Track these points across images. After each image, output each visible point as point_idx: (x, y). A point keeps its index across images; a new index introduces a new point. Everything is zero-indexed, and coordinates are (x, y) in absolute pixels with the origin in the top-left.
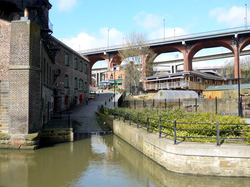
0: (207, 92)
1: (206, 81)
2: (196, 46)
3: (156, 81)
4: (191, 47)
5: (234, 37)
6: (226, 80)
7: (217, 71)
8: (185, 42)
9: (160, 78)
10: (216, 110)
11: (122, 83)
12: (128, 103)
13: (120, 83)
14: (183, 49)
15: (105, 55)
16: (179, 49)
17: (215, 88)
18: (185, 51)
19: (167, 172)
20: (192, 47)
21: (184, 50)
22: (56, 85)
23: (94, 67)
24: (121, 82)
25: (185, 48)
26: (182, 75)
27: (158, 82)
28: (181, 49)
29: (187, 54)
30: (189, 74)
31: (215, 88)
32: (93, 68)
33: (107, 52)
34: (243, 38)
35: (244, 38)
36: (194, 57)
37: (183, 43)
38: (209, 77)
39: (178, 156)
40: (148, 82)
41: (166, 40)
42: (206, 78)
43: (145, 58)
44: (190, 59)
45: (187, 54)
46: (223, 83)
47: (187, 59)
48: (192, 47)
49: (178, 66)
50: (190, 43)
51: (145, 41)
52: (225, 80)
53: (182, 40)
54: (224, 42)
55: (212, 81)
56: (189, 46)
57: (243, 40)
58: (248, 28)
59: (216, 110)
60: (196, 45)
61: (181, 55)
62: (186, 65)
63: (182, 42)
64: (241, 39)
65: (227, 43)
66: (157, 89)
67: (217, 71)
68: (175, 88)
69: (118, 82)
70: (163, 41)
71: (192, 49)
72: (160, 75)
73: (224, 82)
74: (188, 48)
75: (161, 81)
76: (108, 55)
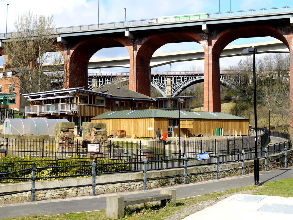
0: (120, 123)
1: (117, 102)
2: (149, 40)
3: (53, 100)
4: (141, 42)
5: (124, 34)
6: (155, 100)
7: (223, 78)
9: (61, 94)
11: (14, 100)
12: (235, 112)
13: (11, 99)
14: (129, 44)
15: (126, 37)
16: (123, 43)
17: (127, 114)
18: (132, 46)
20: (143, 41)
21: (131, 45)
23: (94, 58)
24: (14, 98)
25: (132, 41)
26: (68, 93)
27: (57, 101)
28: (127, 43)
29: (135, 53)
30: (76, 92)
31: (127, 114)
34: (217, 31)
35: (218, 31)
36: (155, 55)
37: (204, 27)
38: (123, 96)
39: (133, 183)
40: (31, 101)
41: (101, 27)
42: (113, 98)
43: (69, 57)
44: (218, 53)
45: (135, 52)
46: (151, 105)
47: (135, 61)
48: (143, 41)
49: (151, 68)
51: (51, 27)
52: (153, 100)
53: (202, 23)
54: (189, 35)
55: (128, 102)
56: (138, 39)
57: (217, 34)
60: (149, 38)
61: (202, 46)
62: (132, 71)
63: (124, 32)
65: (192, 36)
66: (40, 114)
67: (223, 78)
68: (59, 113)
69: (9, 97)
71: (143, 44)
73: (152, 104)
74: (137, 43)
75: (62, 99)
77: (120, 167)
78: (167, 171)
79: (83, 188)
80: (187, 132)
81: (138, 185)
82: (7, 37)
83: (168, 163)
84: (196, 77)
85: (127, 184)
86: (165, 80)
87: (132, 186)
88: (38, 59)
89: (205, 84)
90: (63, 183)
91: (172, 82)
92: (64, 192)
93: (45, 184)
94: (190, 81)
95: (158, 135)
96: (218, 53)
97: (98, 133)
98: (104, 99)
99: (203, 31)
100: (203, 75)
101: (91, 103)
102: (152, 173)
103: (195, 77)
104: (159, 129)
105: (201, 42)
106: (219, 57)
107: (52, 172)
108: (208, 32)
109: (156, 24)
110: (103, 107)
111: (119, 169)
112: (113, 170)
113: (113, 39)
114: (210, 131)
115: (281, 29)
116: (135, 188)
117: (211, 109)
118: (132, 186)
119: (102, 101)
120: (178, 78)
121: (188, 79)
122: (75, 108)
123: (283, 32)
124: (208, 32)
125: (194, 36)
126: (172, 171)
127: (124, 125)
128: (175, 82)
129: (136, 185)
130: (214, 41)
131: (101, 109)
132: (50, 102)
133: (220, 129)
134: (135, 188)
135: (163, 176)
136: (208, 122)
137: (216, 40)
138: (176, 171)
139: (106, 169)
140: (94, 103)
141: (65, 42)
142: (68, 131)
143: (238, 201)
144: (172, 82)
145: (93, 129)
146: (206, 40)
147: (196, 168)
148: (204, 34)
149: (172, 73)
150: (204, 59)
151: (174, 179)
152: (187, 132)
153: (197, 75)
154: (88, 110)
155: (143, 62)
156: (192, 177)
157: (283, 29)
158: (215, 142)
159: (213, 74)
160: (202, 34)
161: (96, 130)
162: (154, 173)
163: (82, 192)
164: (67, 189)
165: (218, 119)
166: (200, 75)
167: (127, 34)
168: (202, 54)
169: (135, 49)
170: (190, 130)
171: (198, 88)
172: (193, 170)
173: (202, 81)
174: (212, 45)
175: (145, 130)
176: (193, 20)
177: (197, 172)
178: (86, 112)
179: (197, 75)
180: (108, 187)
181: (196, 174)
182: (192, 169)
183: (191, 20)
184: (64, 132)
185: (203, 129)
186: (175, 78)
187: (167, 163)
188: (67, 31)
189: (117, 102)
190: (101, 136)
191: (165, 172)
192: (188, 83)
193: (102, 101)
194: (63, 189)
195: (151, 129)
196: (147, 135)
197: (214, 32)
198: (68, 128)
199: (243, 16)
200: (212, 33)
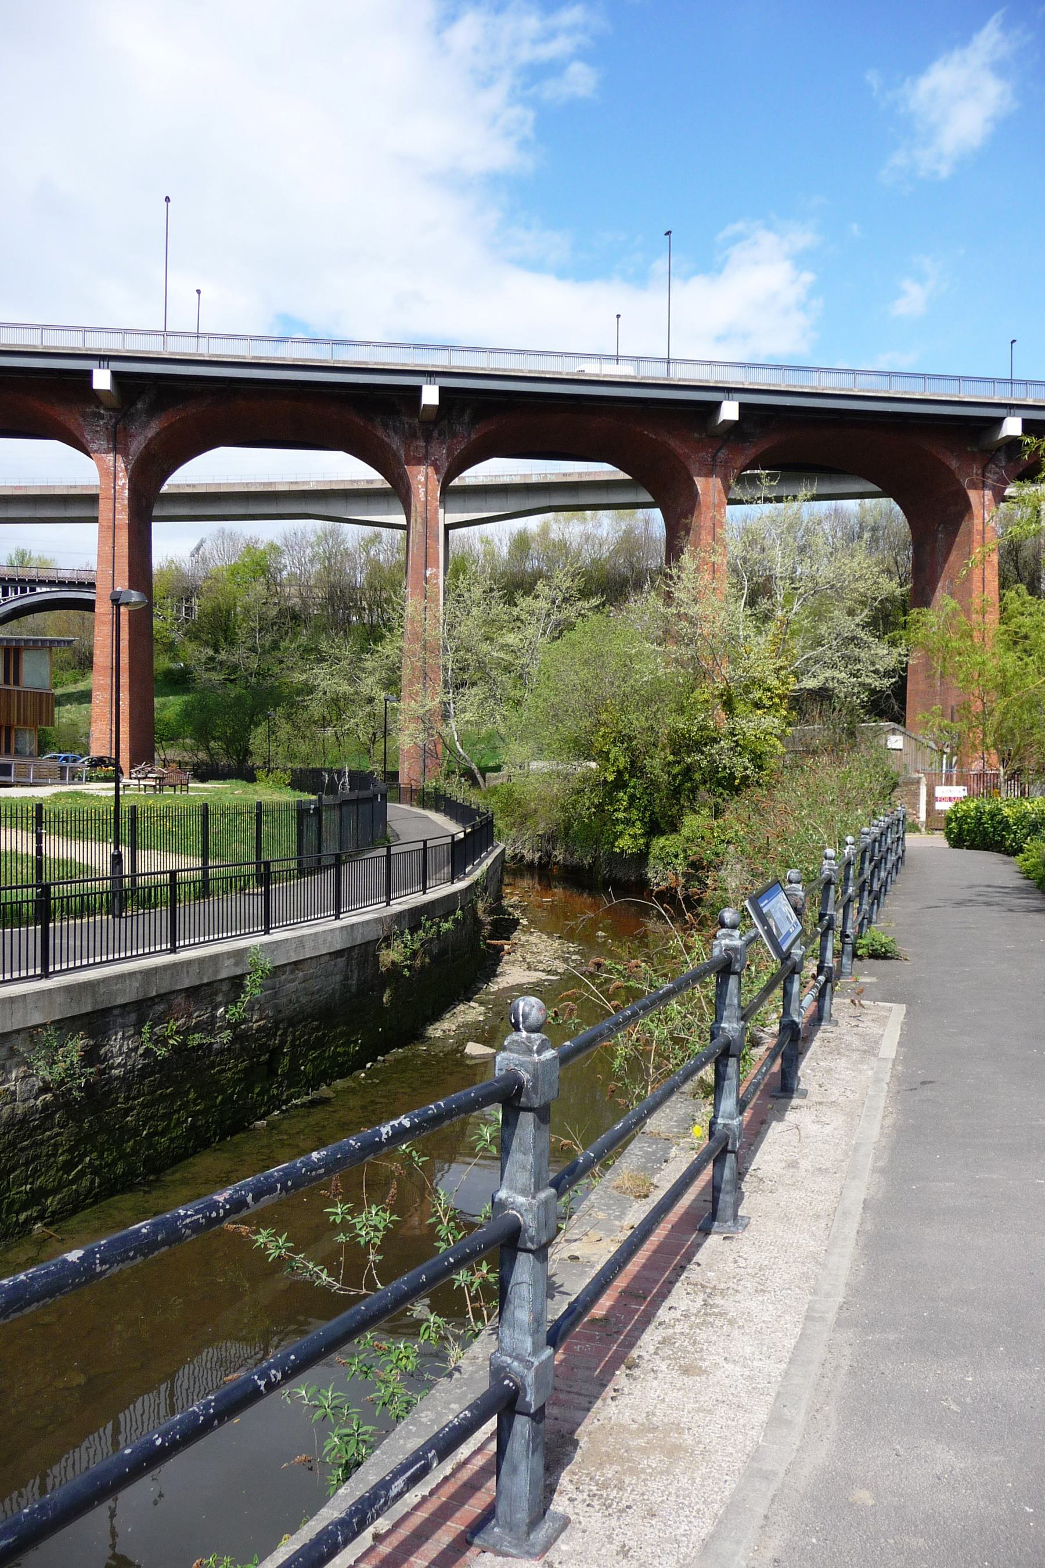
17: (874, 980)
31: (874, 980)
41: (681, 374)
44: (147, 503)
82: (962, 395)
83: (105, 917)
84: (38, 590)
88: (262, 730)
96: (147, 503)
99: (97, 396)
100: (92, 585)
103: (33, 590)
108: (115, 402)
109: (664, 379)
115: (386, 426)
123: (392, 434)
125: (71, 419)
143: (932, 1082)
148: (97, 407)
150: (94, 520)
153: (42, 583)
157: (394, 426)
158: (259, 816)
160: (91, 409)
168: (92, 500)
176: (485, 366)
179: (42, 583)
183: (338, 362)
197: (139, 406)
199: (254, 358)
200: (132, 410)
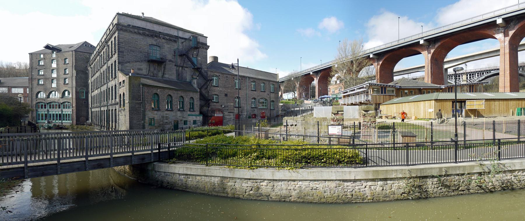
1: (406, 91)
4: (434, 46)
8: (503, 19)
10: (432, 136)
15: (422, 45)
16: (419, 50)
19: (183, 95)
20: (437, 46)
22: (221, 106)
32: (394, 71)
33: (374, 54)
36: (521, 43)
37: (499, 21)
39: (358, 183)
41: (400, 42)
43: (379, 67)
48: (437, 46)
50: (431, 41)
55: (417, 91)
57: (515, 25)
58: (522, 7)
59: (432, 136)
64: (512, 24)
70: (396, 43)
72: (109, 115)
76: (427, 44)
77: (345, 157)
78: (423, 169)
79: (280, 183)
80: (476, 113)
81: (368, 186)
85: (349, 184)
86: (461, 77)
87: (357, 187)
89: (501, 78)
90: (254, 174)
91: (467, 78)
92: (256, 184)
93: (234, 172)
94: (485, 75)
95: (439, 116)
97: (366, 115)
98: (394, 89)
101: (382, 93)
102: (392, 170)
104: (440, 110)
105: (496, 36)
106: (517, 51)
107: (258, 157)
110: (393, 96)
111: (344, 161)
112: (333, 161)
113: (410, 49)
114: (507, 111)
116: (362, 190)
117: (508, 89)
118: (357, 187)
119: (393, 91)
120: (473, 74)
121: (483, 74)
122: (370, 98)
124: (504, 25)
125: (489, 32)
126: (431, 168)
127: (407, 108)
128: (470, 77)
129: (364, 186)
130: (511, 33)
131: (391, 97)
132: (354, 95)
133: (521, 109)
134: (362, 190)
135: (414, 175)
136: (505, 102)
137: (513, 31)
138: (441, 169)
139: (323, 159)
140: (385, 93)
141: (375, 57)
142: (338, 114)
144: (467, 78)
145: (362, 111)
146: (502, 32)
147: (481, 165)
149: (468, 71)
151: (436, 179)
152: (476, 113)
153: (492, 70)
154: (380, 98)
155: (437, 62)
156: (473, 178)
159: (510, 62)
161: (364, 112)
162: (397, 170)
163: (279, 187)
164: (259, 181)
165: (518, 99)
166: (495, 70)
167: (422, 42)
168: (498, 51)
169: (429, 53)
170: (480, 111)
171: (493, 81)
172: (476, 168)
173: (498, 74)
174: (508, 36)
175: (425, 112)
177: (481, 171)
178: (378, 100)
179: (492, 70)
180: (317, 186)
181: (480, 174)
182: (473, 166)
184: (334, 114)
185: (497, 109)
186: (470, 75)
187: (436, 150)
188: (376, 49)
189: (406, 91)
190: (369, 118)
191: (417, 169)
192: (483, 77)
193: (393, 91)
194: (254, 181)
195: (432, 110)
196: (428, 117)
198: (338, 111)
